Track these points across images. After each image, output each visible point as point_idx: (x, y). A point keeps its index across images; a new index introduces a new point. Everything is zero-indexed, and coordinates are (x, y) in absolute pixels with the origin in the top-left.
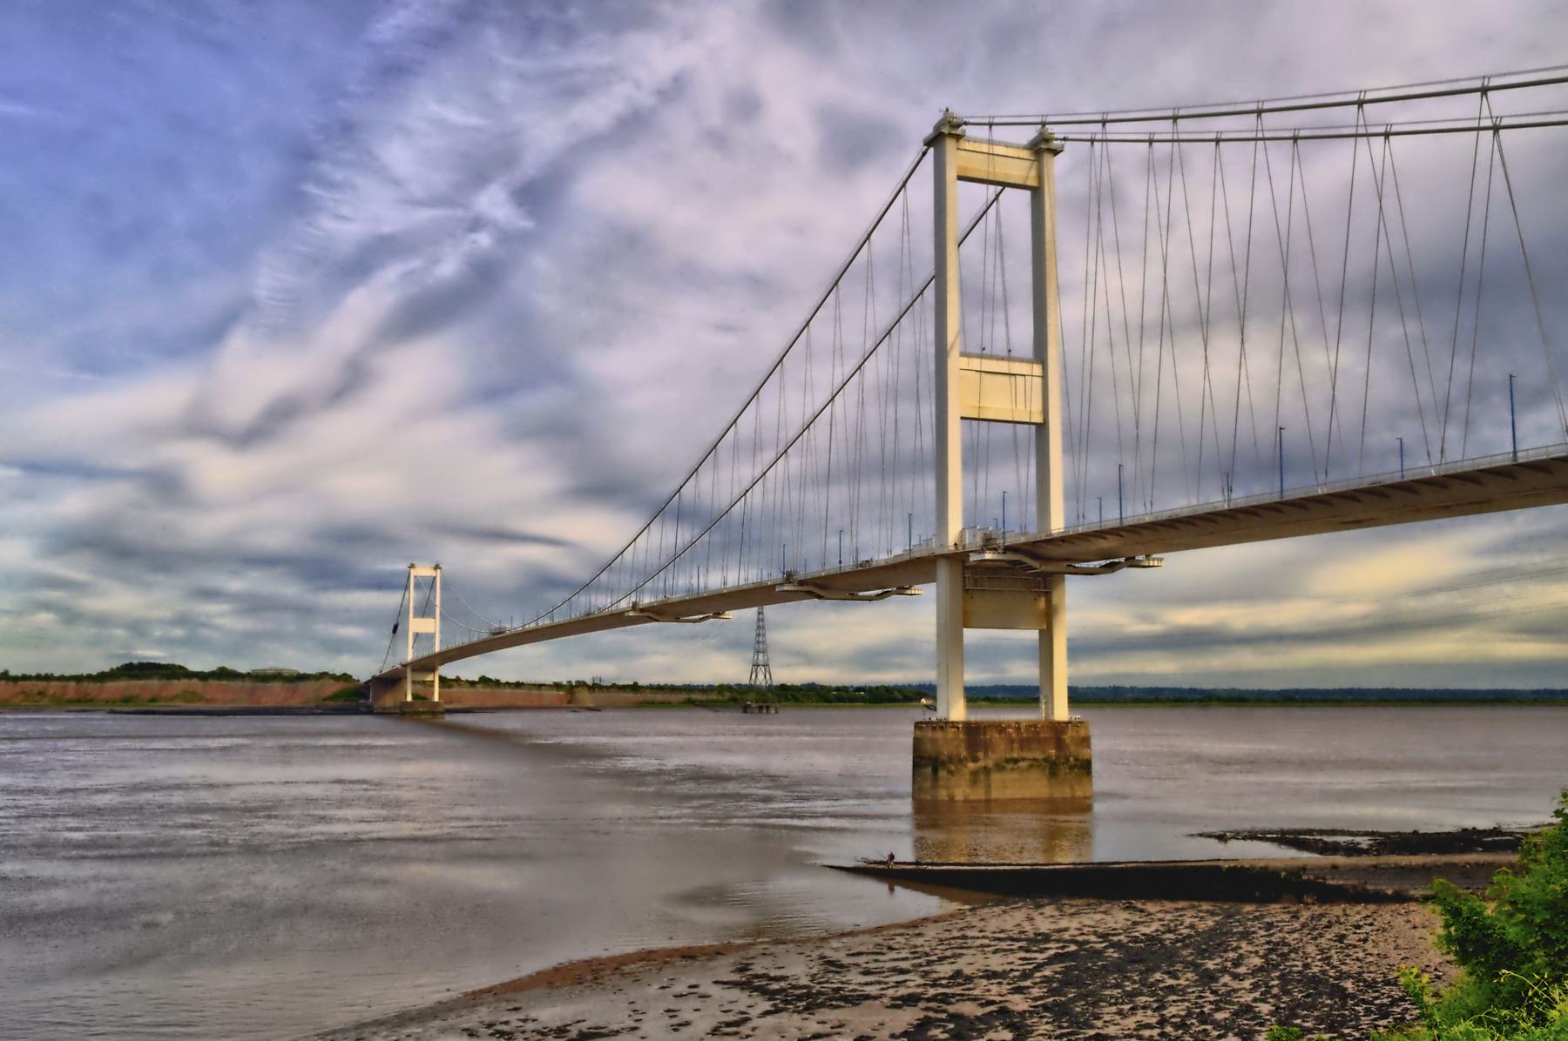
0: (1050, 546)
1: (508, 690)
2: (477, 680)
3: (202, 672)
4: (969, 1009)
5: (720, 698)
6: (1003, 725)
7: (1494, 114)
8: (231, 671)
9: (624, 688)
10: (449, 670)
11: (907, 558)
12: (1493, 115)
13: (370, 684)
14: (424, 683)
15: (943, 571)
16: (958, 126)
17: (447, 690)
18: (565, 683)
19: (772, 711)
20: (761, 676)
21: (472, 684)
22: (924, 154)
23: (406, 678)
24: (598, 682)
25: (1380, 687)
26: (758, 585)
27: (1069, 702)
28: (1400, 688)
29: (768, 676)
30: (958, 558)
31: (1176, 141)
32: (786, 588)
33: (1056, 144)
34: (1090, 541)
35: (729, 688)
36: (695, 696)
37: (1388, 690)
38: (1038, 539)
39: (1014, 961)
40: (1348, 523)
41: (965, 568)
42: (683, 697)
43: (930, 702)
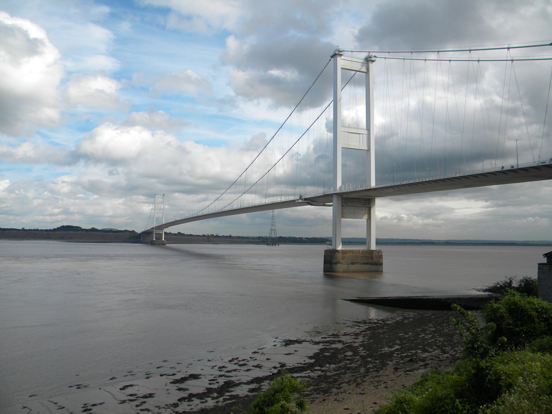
0: (370, 191)
1: (187, 237)
2: (177, 233)
3: (86, 229)
4: (339, 346)
5: (259, 241)
6: (354, 251)
7: (512, 56)
8: (96, 229)
9: (226, 237)
10: (168, 230)
11: (265, 204)
12: (511, 56)
13: (141, 234)
14: (159, 234)
15: (335, 199)
16: (341, 51)
17: (166, 236)
18: (206, 235)
19: (277, 245)
20: (273, 234)
21: (176, 234)
22: (330, 60)
23: (153, 232)
24: (218, 235)
25: (312, 237)
26: (273, 203)
27: (376, 243)
28: (444, 240)
29: (275, 234)
30: (341, 195)
31: (412, 59)
32: (300, 201)
33: (373, 59)
34: (383, 190)
35: (262, 238)
36: (250, 240)
37: (352, 238)
38: (367, 189)
39: (356, 330)
40: (466, 186)
41: (342, 198)
42: (247, 240)
43: (330, 243)
